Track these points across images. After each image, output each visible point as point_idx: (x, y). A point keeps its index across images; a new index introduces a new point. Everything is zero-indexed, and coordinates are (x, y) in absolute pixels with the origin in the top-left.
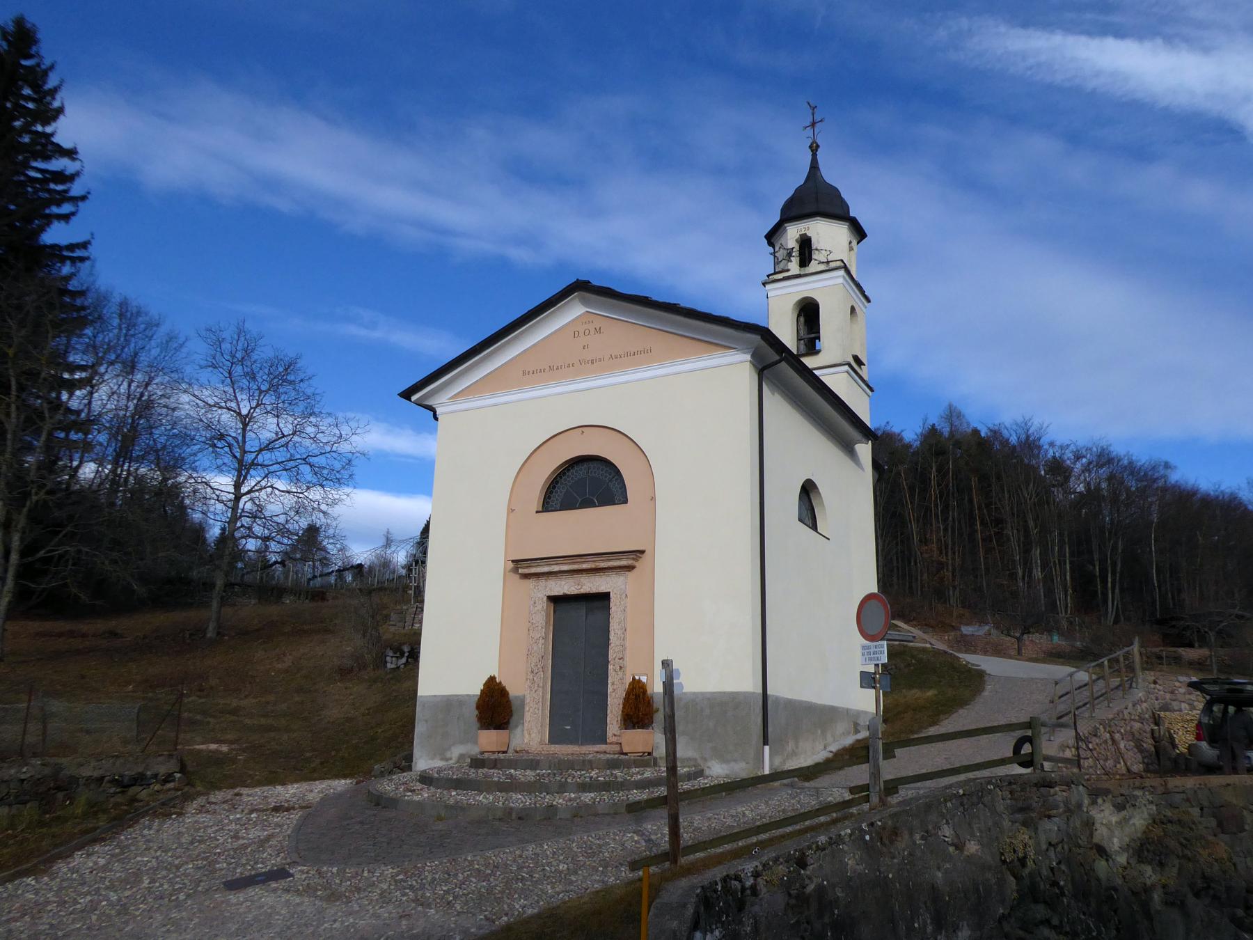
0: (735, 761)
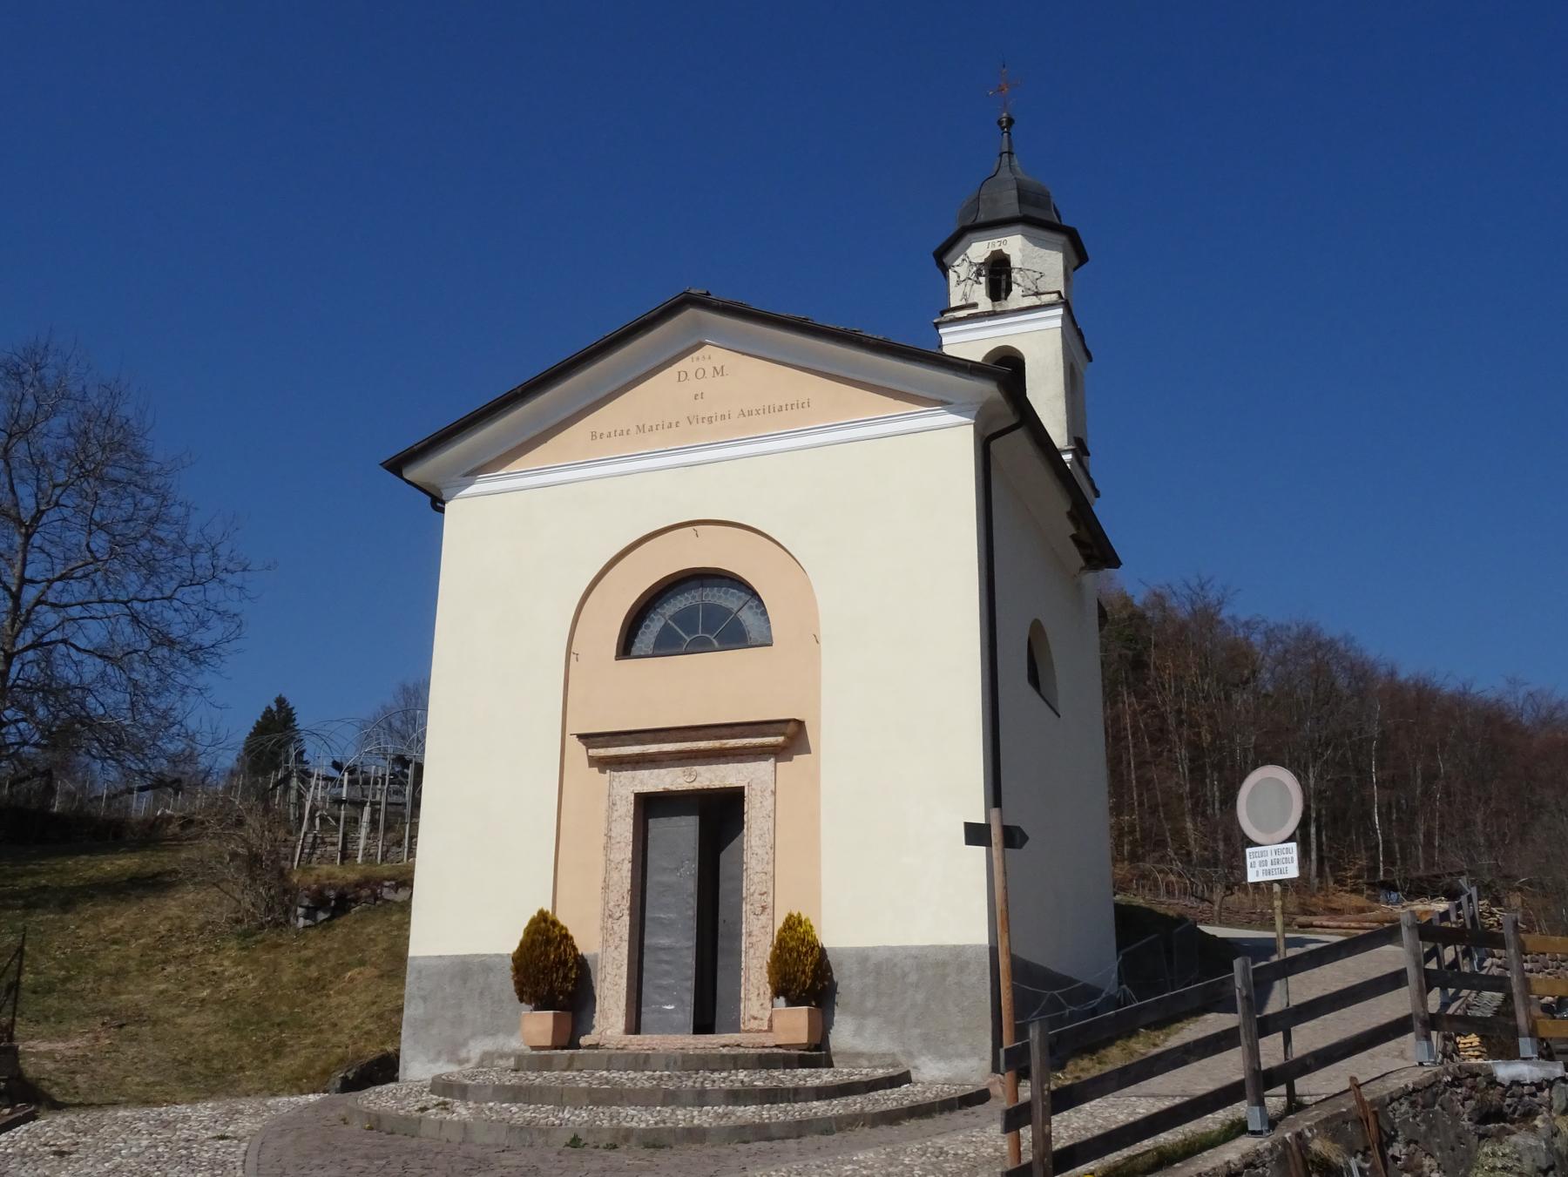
0: (961, 1056)
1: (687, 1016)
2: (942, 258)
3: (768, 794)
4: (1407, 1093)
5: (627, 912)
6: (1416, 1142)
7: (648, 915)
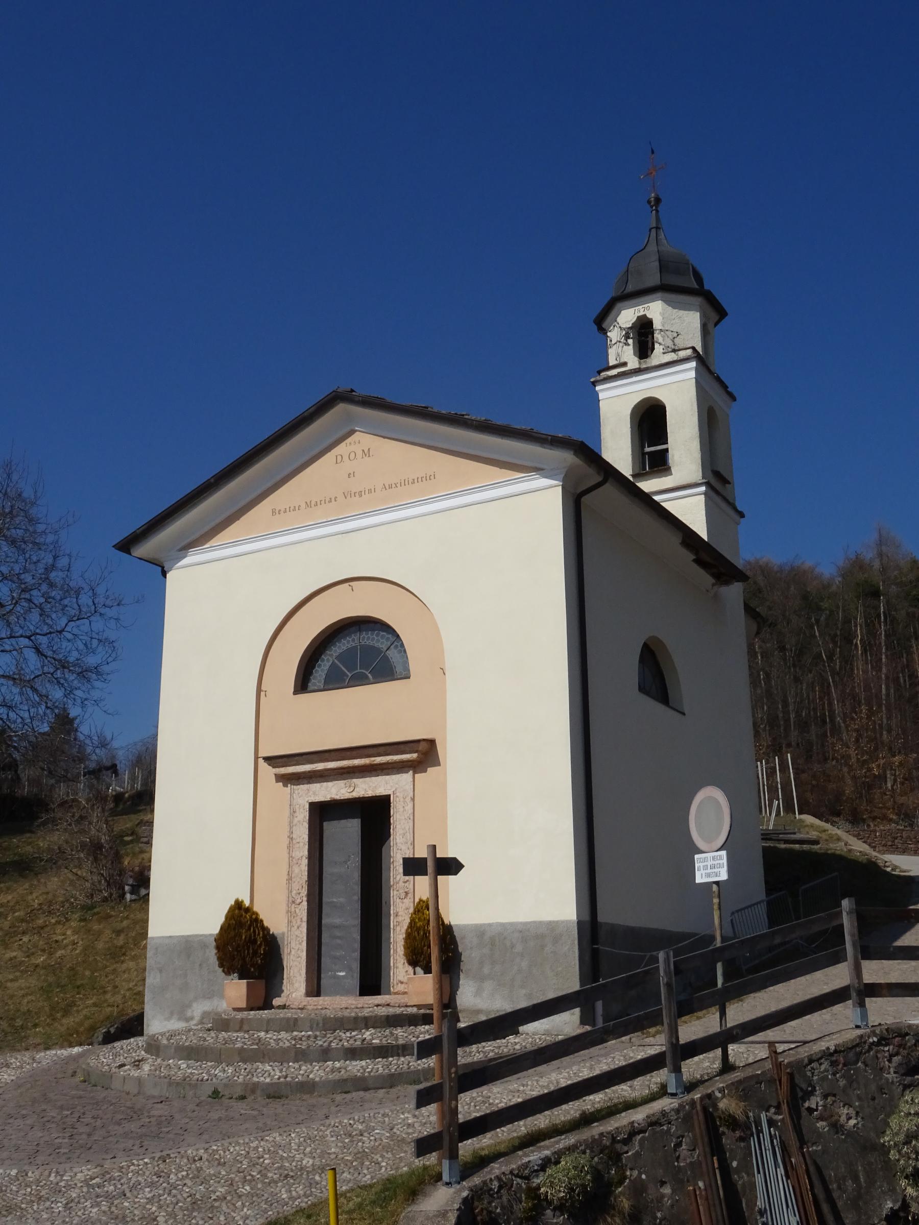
1: (355, 982)
2: (601, 321)
3: (408, 799)
4: (827, 1054)
5: (305, 899)
6: (834, 1095)
7: (325, 899)
